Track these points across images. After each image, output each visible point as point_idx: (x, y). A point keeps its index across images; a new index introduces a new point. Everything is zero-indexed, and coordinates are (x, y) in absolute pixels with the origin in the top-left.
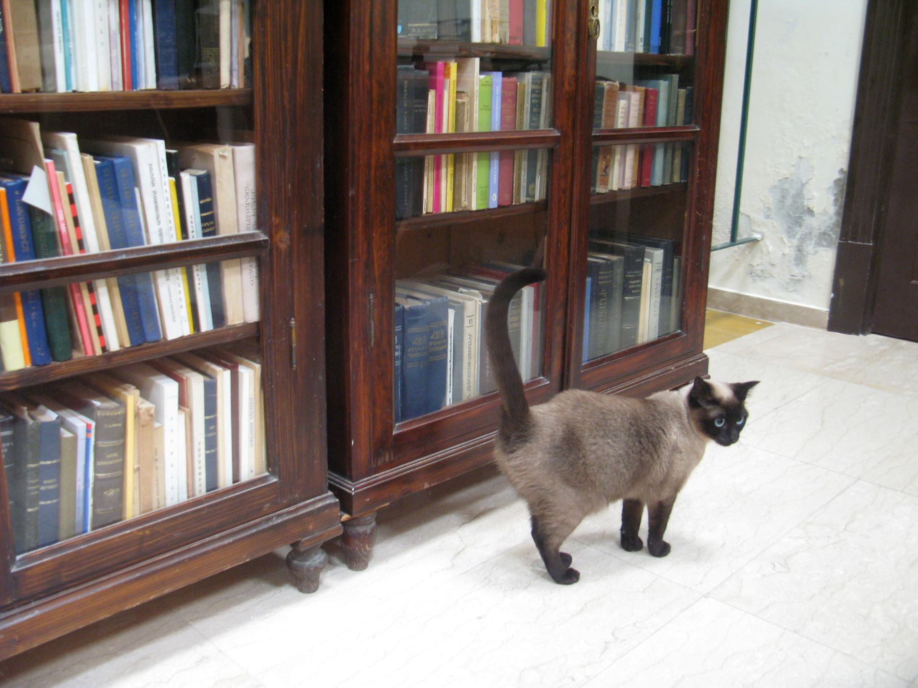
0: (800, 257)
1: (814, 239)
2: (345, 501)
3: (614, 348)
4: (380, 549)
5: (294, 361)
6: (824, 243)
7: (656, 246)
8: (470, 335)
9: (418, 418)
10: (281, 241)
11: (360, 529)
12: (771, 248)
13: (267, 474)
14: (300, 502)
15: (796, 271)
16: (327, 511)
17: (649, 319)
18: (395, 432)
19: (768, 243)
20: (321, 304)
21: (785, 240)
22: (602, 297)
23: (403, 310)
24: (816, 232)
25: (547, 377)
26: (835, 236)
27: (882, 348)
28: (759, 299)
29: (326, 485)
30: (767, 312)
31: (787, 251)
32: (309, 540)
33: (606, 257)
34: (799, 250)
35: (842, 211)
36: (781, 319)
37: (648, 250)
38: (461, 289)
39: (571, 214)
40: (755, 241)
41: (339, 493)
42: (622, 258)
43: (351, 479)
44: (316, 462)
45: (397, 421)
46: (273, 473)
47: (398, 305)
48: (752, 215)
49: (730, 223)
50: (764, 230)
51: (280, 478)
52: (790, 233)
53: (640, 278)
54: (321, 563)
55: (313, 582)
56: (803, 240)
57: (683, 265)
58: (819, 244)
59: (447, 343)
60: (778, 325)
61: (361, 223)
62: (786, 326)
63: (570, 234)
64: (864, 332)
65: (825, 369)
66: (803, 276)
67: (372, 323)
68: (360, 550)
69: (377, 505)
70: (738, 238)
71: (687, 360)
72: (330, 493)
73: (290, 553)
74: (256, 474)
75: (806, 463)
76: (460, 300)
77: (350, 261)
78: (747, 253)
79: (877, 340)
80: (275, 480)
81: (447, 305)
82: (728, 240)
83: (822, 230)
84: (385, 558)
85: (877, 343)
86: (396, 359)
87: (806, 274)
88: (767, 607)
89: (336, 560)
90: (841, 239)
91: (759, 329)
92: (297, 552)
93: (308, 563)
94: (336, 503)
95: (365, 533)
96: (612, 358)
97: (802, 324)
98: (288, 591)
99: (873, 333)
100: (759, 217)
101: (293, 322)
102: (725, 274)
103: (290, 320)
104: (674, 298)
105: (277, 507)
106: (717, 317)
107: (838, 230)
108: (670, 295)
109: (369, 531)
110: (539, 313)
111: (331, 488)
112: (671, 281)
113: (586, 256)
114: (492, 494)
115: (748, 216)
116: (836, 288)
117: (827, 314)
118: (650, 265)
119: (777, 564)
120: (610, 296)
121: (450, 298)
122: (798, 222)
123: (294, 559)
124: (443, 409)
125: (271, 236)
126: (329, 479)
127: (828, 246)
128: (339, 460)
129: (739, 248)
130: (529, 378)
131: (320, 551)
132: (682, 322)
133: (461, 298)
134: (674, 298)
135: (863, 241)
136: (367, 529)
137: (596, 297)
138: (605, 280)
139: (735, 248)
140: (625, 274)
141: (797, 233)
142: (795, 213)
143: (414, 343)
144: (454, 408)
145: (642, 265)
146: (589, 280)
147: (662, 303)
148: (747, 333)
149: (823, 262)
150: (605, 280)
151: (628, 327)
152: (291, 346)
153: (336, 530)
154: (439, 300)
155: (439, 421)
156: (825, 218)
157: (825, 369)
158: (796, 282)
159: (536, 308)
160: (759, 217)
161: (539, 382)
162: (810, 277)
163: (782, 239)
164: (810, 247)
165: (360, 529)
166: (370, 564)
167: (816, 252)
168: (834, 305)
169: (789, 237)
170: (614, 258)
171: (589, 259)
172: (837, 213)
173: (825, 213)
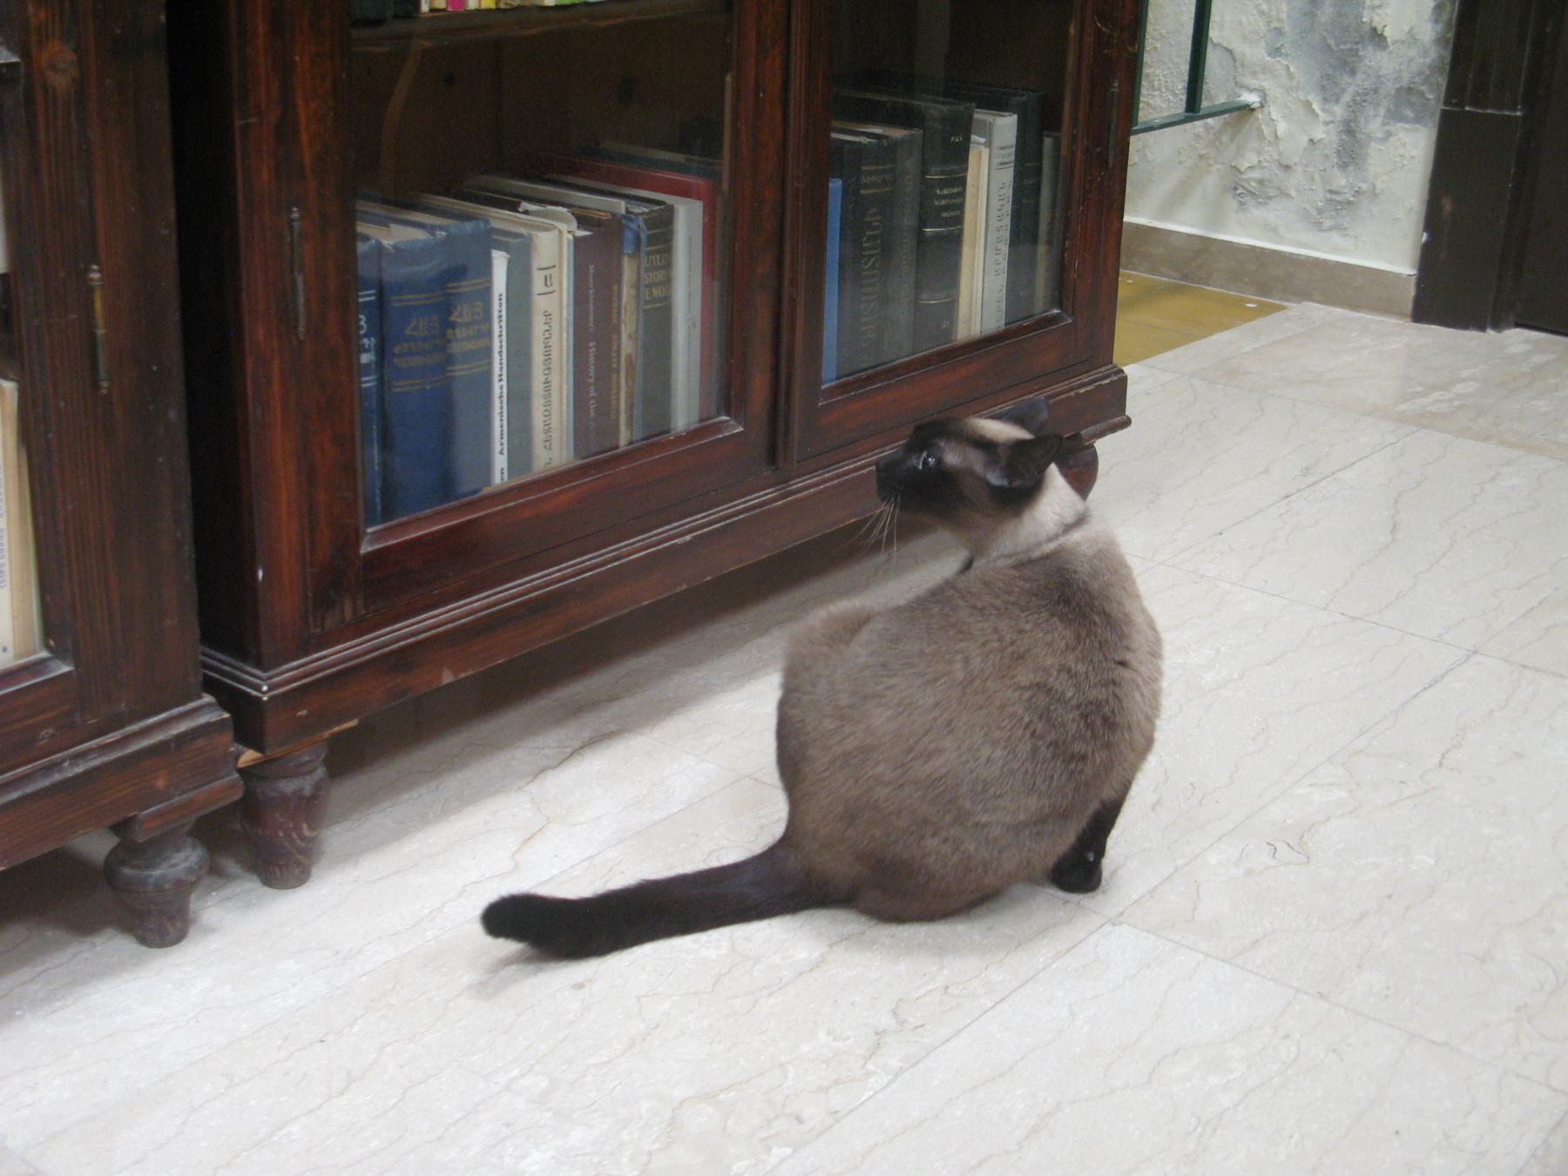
0: (1351, 149)
1: (1385, 103)
2: (246, 719)
3: (900, 346)
4: (335, 837)
5: (103, 373)
6: (1409, 113)
7: (1000, 106)
8: (547, 315)
9: (421, 514)
10: (54, 68)
11: (288, 786)
12: (1282, 127)
13: (44, 654)
14: (131, 721)
15: (1340, 180)
16: (201, 742)
17: (982, 291)
18: (365, 549)
19: (1274, 115)
20: (167, 231)
21: (1315, 106)
22: (870, 226)
23: (379, 248)
24: (1389, 88)
25: (736, 418)
26: (1434, 98)
27: (1538, 359)
28: (1253, 248)
29: (196, 679)
30: (1270, 281)
31: (1319, 133)
32: (159, 814)
33: (878, 130)
34: (1350, 130)
35: (1450, 35)
36: (1305, 295)
37: (980, 115)
38: (525, 205)
39: (789, 17)
40: (1247, 109)
41: (230, 698)
42: (917, 133)
43: (259, 664)
44: (169, 622)
45: (370, 523)
46: (59, 653)
47: (366, 238)
48: (1239, 47)
49: (1185, 68)
50: (1265, 84)
51: (77, 666)
52: (1329, 91)
53: (962, 182)
54: (189, 870)
55: (172, 919)
56: (1356, 106)
57: (1064, 152)
58: (1395, 115)
59: (489, 334)
60: (1295, 308)
61: (261, 29)
62: (1316, 311)
63: (786, 68)
64: (1498, 325)
65: (1404, 407)
66: (1358, 193)
67: (300, 279)
68: (292, 842)
69: (328, 726)
70: (1205, 104)
71: (1076, 382)
72: (208, 698)
73: (114, 850)
74: (17, 657)
75: (1354, 618)
76: (523, 230)
77: (238, 123)
78: (1225, 139)
79: (1527, 341)
80: (66, 669)
81: (489, 240)
82: (1178, 105)
83: (1405, 82)
84: (353, 855)
85: (1528, 347)
86: (366, 369)
87: (1364, 186)
88: (1256, 942)
89: (231, 866)
90: (1447, 103)
91: (1254, 318)
92: (134, 848)
93: (157, 873)
94: (223, 720)
95: (298, 794)
96: (893, 372)
97: (1354, 307)
98: (114, 945)
99: (1517, 325)
100: (1255, 53)
101: (96, 276)
102: (1168, 188)
103: (87, 270)
104: (1042, 249)
105: (72, 733)
106: (1150, 293)
107: (1443, 82)
108: (1034, 240)
109: (308, 791)
110: (716, 284)
111: (210, 686)
112: (1037, 189)
113: (828, 130)
114: (613, 698)
115: (1230, 51)
116: (1433, 219)
117: (1413, 280)
118: (985, 152)
119: (1280, 846)
120: (887, 249)
121: (495, 224)
122: (1348, 63)
123: (123, 863)
124: (486, 491)
125: (25, 53)
126: (205, 666)
127: (1417, 120)
128: (227, 615)
129: (1207, 128)
130: (695, 417)
131: (190, 840)
132: (1061, 291)
133: (525, 225)
134: (1042, 249)
135: (1501, 108)
136: (306, 784)
137: (853, 226)
138: (874, 185)
139: (1198, 126)
140: (924, 173)
141: (1344, 91)
142: (1341, 45)
143: (408, 332)
144: (511, 490)
145: (967, 150)
146: (835, 185)
147: (1013, 265)
148: (1222, 327)
149: (1405, 156)
150: (874, 185)
151: (930, 300)
152: (92, 336)
153: (224, 788)
154: (469, 226)
155: (470, 522)
156: (1413, 52)
157: (1404, 407)
158: (1339, 208)
159: (709, 270)
160: (1255, 53)
161: (718, 427)
162: (1374, 194)
163: (1308, 105)
164: (1374, 125)
165: (288, 786)
166: (314, 870)
167: (1389, 134)
168: (1429, 259)
169: (1326, 100)
170: (897, 133)
171: (834, 135)
172: (1441, 40)
173: (1411, 38)
